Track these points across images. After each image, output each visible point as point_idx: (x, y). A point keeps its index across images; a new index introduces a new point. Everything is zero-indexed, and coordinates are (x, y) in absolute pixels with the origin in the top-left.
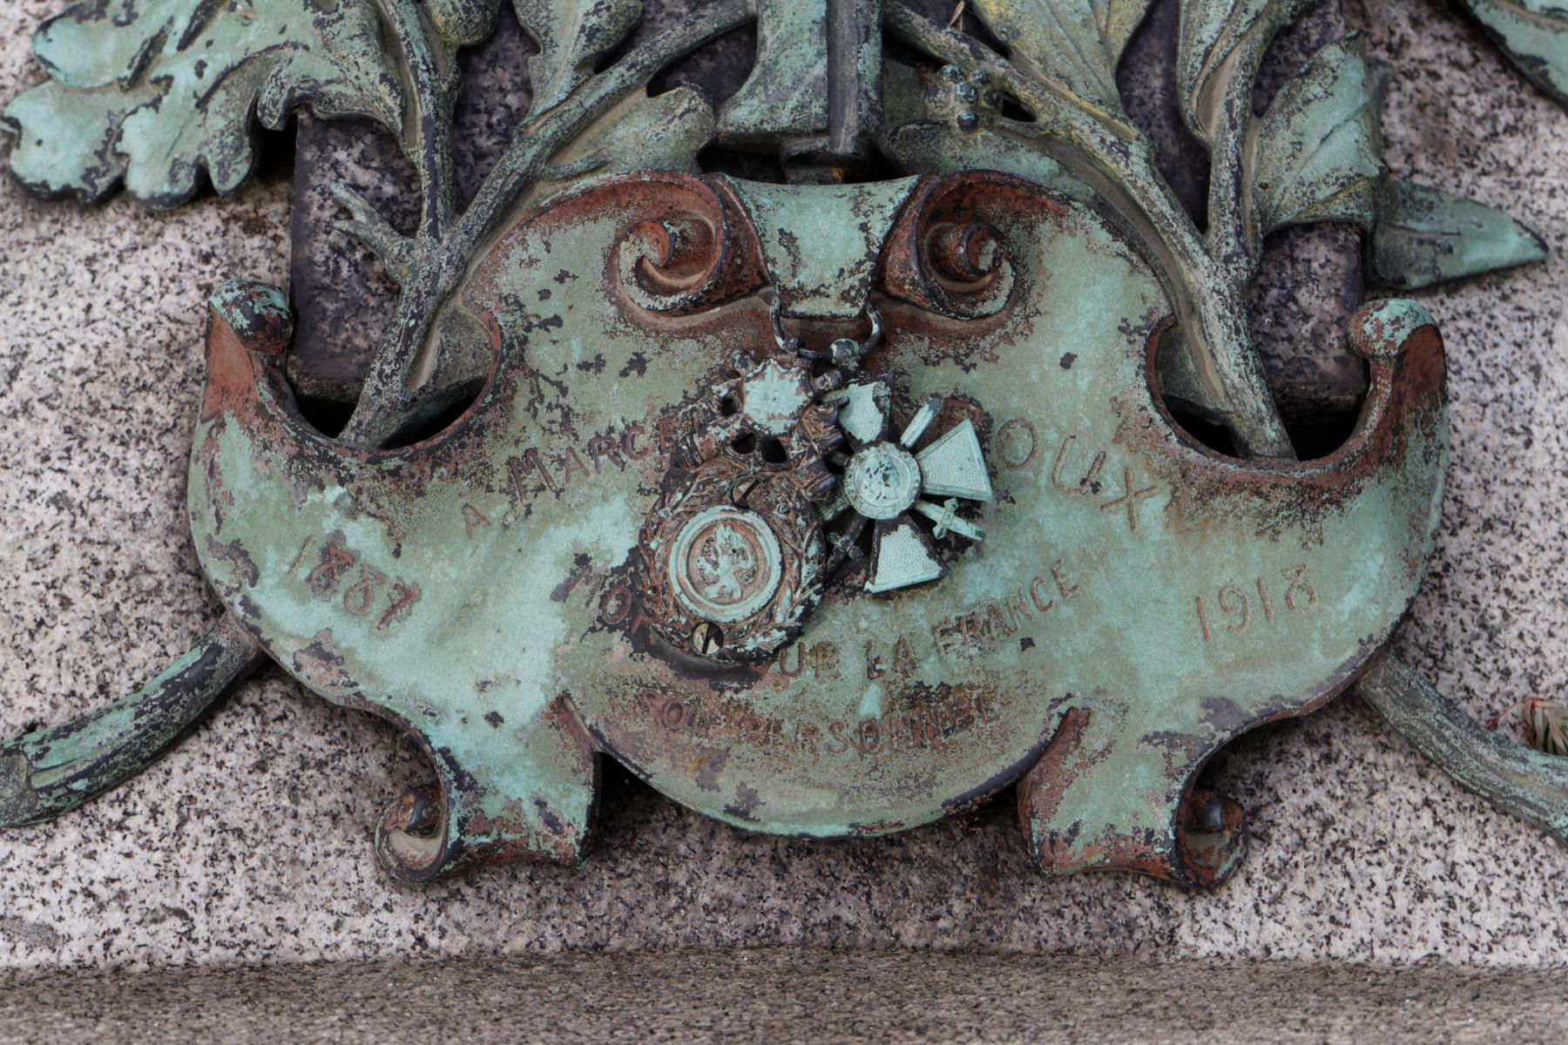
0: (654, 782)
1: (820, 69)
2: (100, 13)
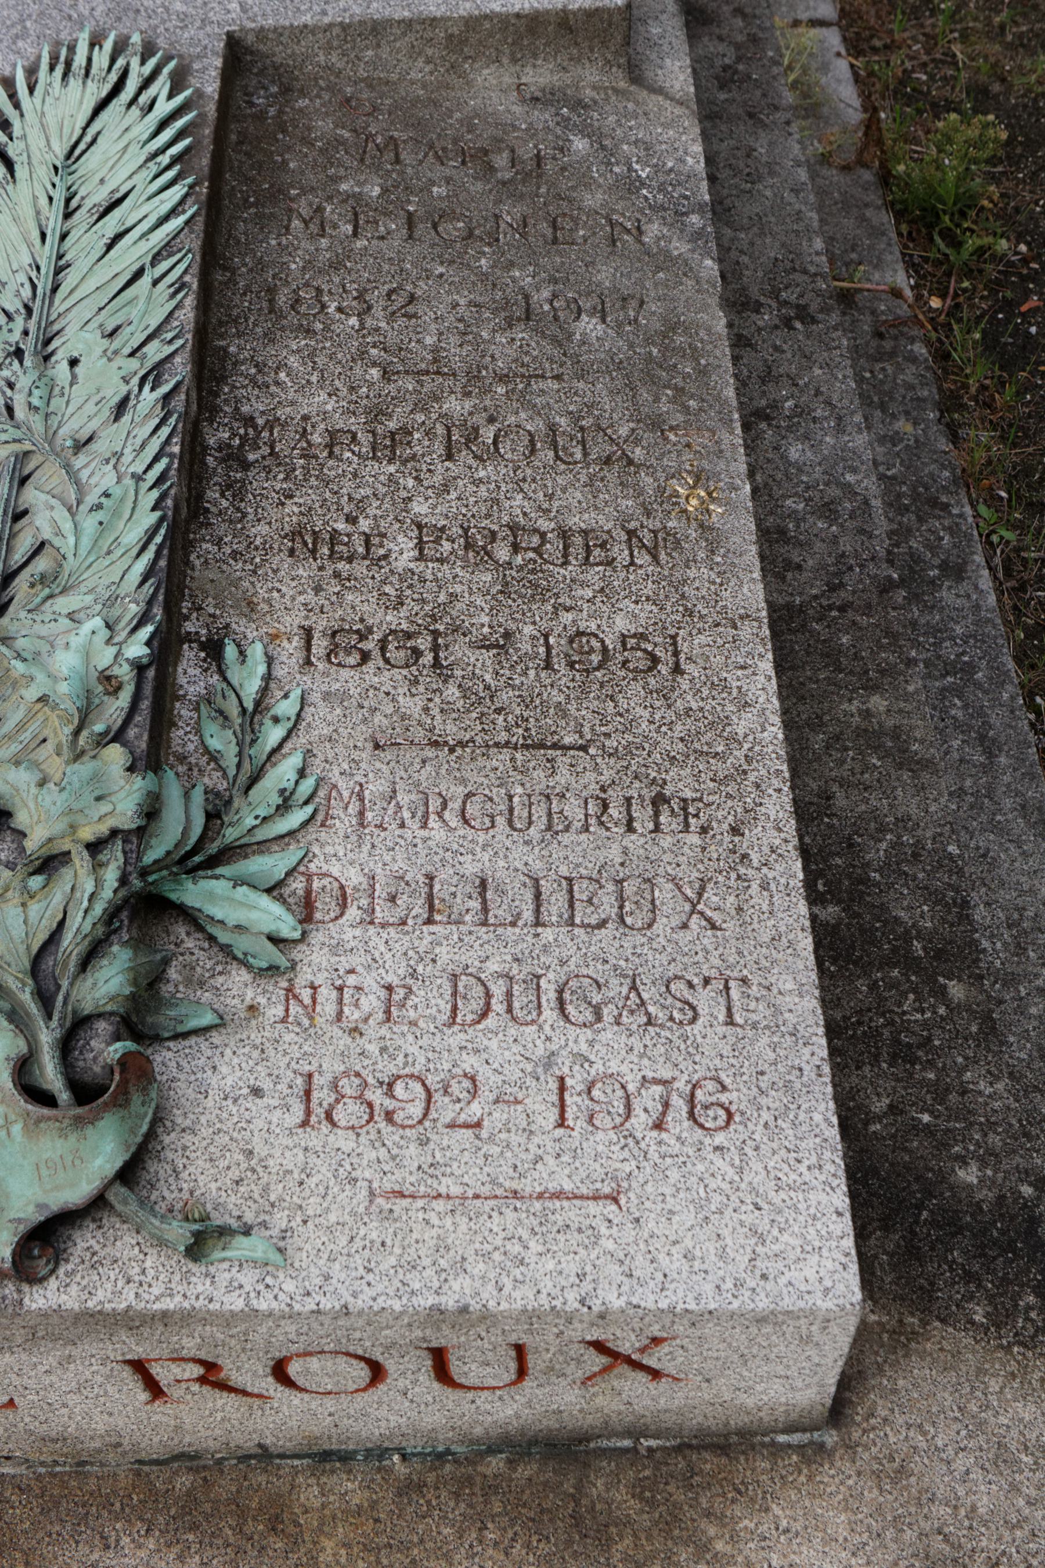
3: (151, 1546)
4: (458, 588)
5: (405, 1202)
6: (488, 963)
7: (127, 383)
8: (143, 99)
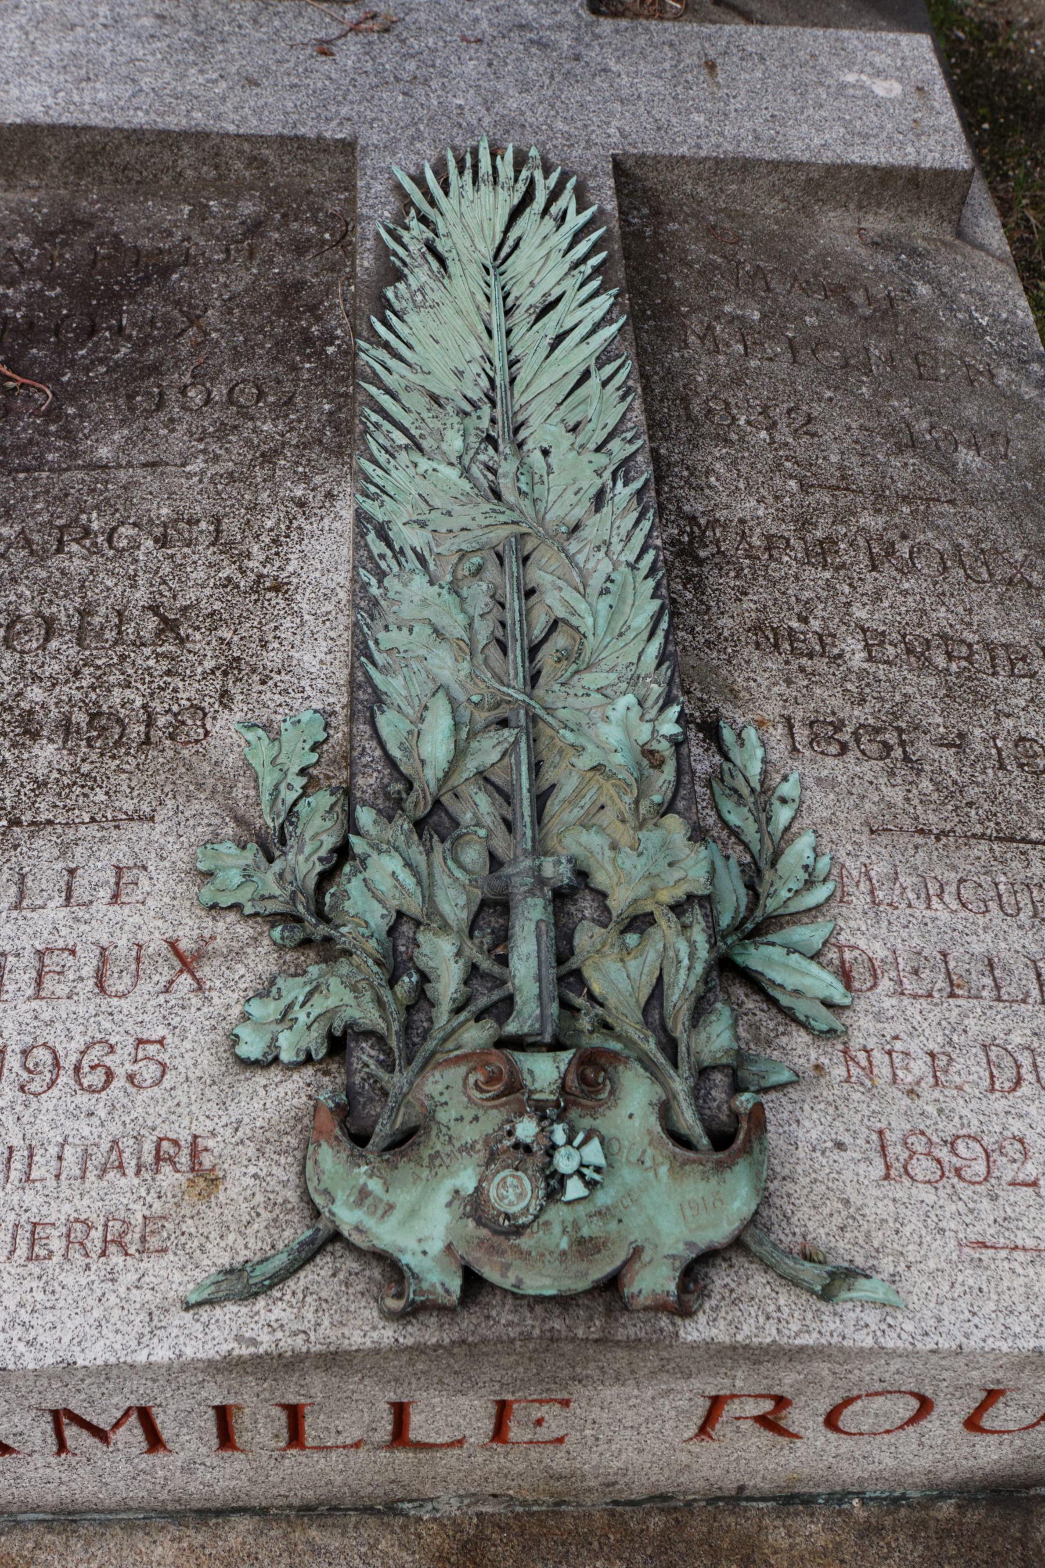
0: (485, 1276)
1: (538, 1012)
2: (268, 996)
4: (910, 690)
5: (990, 1252)
6: (1012, 1036)
7: (600, 475)
8: (554, 210)
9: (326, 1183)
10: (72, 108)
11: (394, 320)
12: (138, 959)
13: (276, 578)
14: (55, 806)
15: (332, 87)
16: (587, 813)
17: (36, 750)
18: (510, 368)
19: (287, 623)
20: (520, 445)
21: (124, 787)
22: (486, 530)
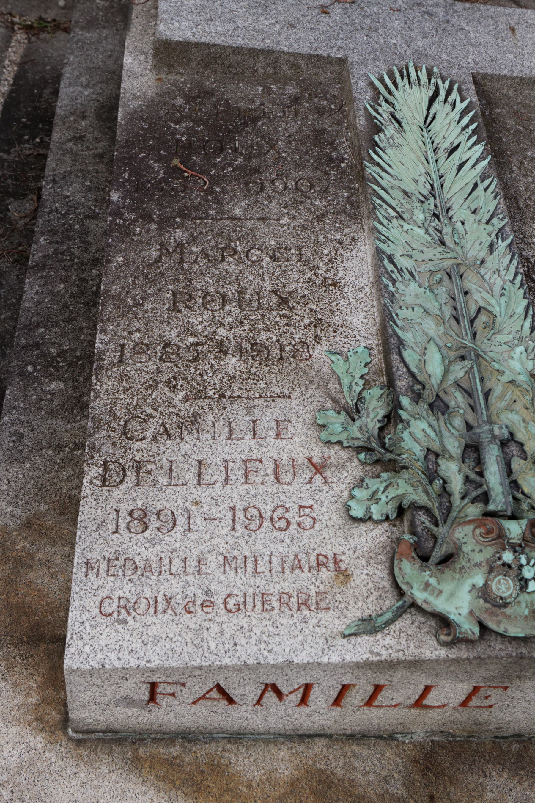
3: (506, 777)
7: (490, 236)
8: (450, 99)
9: (407, 579)
10: (206, 34)
11: (381, 153)
12: (293, 466)
13: (333, 279)
14: (241, 389)
15: (331, 30)
16: (508, 404)
17: (227, 360)
18: (440, 178)
19: (342, 302)
20: (451, 218)
21: (274, 381)
22: (441, 261)
